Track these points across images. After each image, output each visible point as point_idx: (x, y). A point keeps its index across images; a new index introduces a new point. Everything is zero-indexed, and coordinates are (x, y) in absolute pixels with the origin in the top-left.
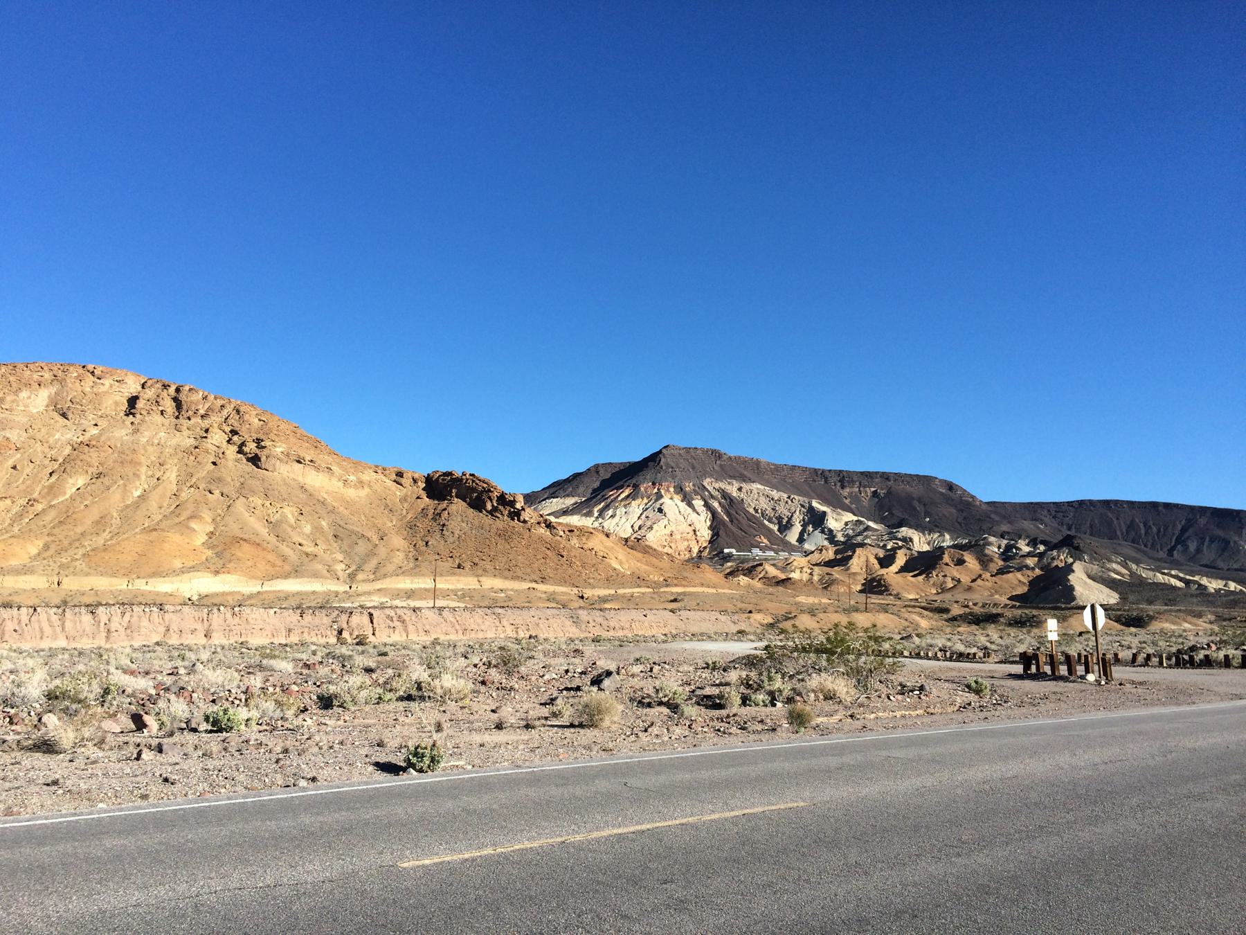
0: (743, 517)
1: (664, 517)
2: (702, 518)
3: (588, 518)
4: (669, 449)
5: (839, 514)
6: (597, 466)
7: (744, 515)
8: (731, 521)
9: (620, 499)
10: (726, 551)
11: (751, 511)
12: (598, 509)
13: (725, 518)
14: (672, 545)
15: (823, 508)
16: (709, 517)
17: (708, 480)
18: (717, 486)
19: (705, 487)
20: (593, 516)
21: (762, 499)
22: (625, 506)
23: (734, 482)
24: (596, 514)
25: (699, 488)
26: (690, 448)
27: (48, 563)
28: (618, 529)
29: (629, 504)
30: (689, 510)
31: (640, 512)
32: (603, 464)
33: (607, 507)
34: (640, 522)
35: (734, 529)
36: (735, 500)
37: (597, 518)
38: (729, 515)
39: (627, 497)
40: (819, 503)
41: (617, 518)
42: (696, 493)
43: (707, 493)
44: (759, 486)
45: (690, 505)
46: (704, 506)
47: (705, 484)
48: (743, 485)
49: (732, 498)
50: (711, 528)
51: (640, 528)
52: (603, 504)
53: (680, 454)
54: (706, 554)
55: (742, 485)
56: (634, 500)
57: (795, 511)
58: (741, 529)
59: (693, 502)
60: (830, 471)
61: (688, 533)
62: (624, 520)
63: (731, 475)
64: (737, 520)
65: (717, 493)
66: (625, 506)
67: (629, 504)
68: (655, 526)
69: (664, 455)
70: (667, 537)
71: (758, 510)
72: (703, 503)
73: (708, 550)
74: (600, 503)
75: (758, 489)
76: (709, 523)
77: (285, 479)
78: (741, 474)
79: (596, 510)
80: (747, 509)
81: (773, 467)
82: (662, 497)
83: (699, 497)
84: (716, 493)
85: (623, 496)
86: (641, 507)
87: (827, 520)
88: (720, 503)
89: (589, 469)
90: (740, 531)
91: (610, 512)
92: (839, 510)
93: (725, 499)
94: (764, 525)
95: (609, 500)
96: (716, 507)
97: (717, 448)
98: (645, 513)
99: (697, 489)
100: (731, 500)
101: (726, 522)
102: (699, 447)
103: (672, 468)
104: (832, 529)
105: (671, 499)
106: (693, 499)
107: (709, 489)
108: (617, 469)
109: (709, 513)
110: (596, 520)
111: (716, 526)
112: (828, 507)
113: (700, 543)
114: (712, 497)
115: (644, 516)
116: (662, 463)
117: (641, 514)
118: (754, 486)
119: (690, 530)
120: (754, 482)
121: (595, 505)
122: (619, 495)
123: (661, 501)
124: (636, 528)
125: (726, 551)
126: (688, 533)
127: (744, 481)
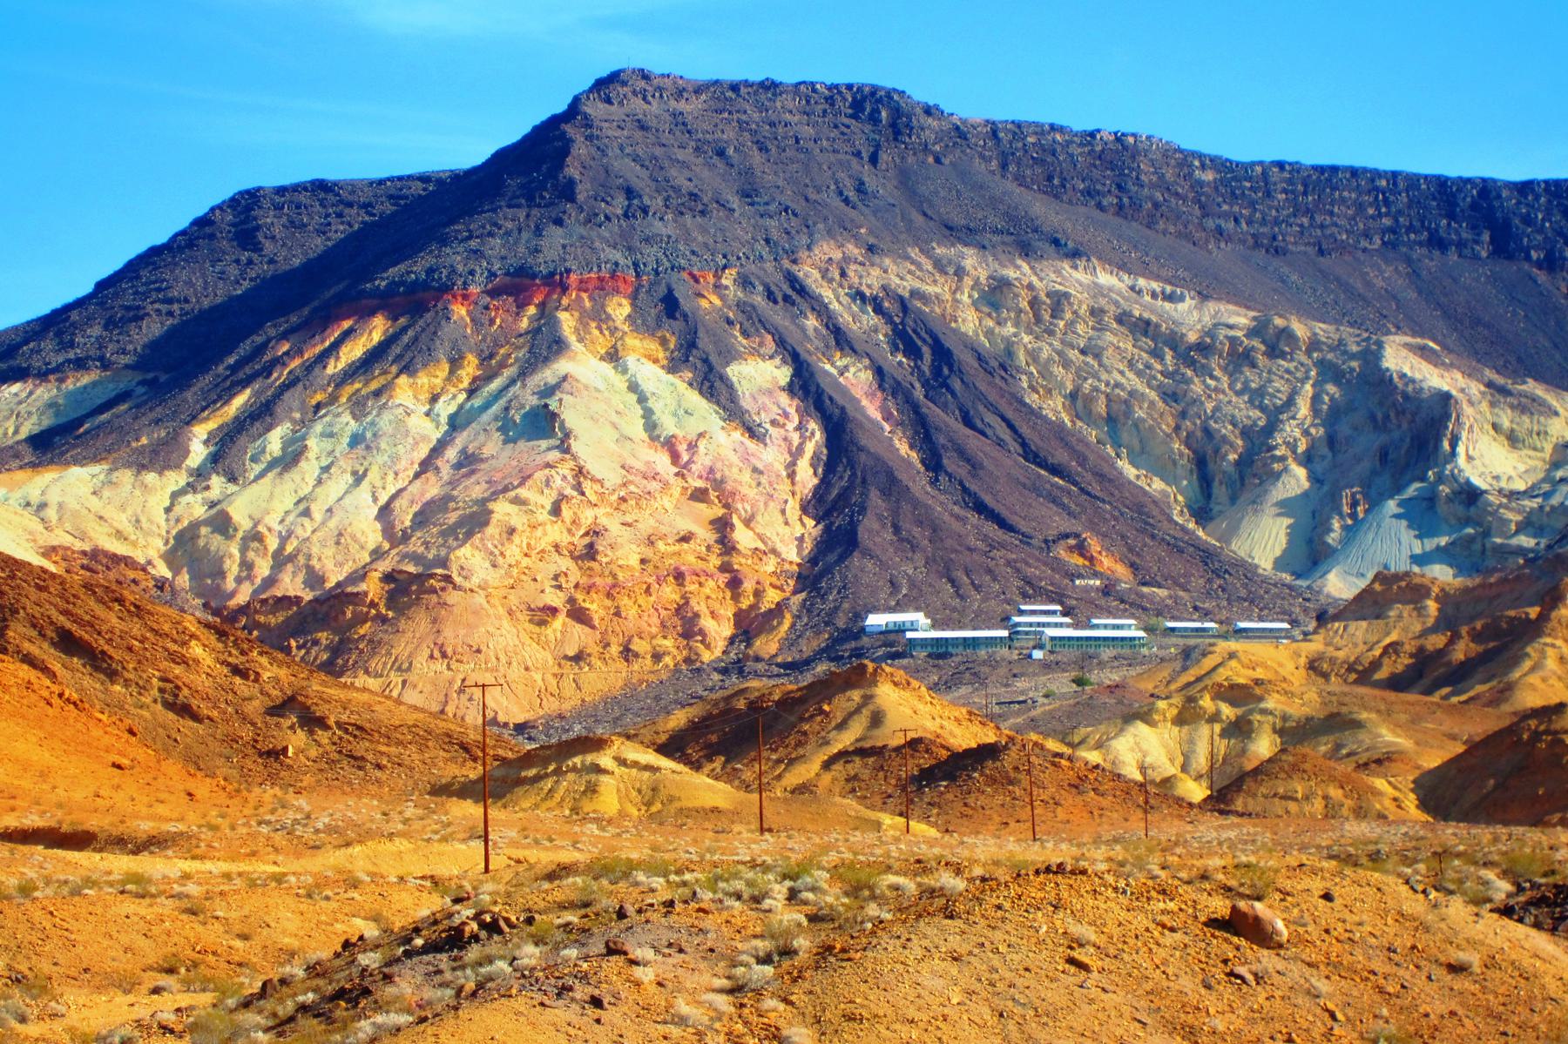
0: (1000, 443)
1: (554, 455)
2: (772, 456)
3: (150, 477)
4: (617, 91)
5: (1528, 406)
6: (246, 203)
7: (1005, 434)
8: (933, 463)
9: (334, 367)
10: (876, 620)
11: (1054, 408)
12: (212, 425)
13: (903, 448)
14: (595, 606)
15: (1435, 379)
16: (810, 448)
17: (827, 250)
18: (872, 280)
19: (802, 291)
20: (178, 466)
21: (1117, 341)
22: (358, 407)
23: (970, 259)
24: (198, 452)
25: (771, 296)
26: (735, 87)
27: (1336, 1026)
28: (305, 529)
29: (377, 394)
30: (704, 413)
31: (436, 435)
32: (281, 191)
33: (261, 415)
34: (432, 488)
35: (942, 504)
36: (966, 358)
37: (200, 474)
38: (923, 433)
39: (374, 357)
40: (1423, 352)
41: (309, 468)
42: (752, 321)
43: (812, 322)
44: (1105, 278)
45: (713, 384)
46: (790, 389)
47: (809, 273)
48: (1020, 271)
49: (948, 343)
50: (820, 505)
51: (423, 518)
52: (240, 401)
53: (677, 118)
54: (773, 647)
55: (1011, 273)
56: (408, 369)
57: (1290, 402)
58: (980, 508)
59: (734, 371)
60: (1525, 188)
61: (685, 539)
62: (339, 483)
63: (959, 220)
64: (962, 453)
65: (870, 319)
66: (358, 407)
67: (377, 394)
68: (502, 509)
69: (588, 123)
70: (565, 563)
71: (1089, 400)
72: (784, 374)
73: (787, 621)
74: (226, 395)
75: (1098, 291)
76: (807, 478)
77: (732, 598)
78: (1010, 217)
79: (201, 431)
80: (1032, 399)
81: (1209, 176)
82: (558, 346)
83: (770, 345)
84: (862, 323)
85: (353, 351)
86: (446, 408)
87: (1454, 443)
88: (879, 372)
89: (201, 222)
90: (973, 518)
91: (274, 442)
92: (1532, 387)
93: (912, 351)
94: (1111, 480)
95: (280, 376)
96: (858, 393)
97: (886, 81)
98: (461, 440)
99: (759, 300)
100: (942, 354)
101: (902, 476)
102: (787, 76)
103: (630, 193)
104: (1477, 481)
105: (613, 356)
106: (731, 355)
107: (827, 294)
108: (357, 218)
109: (813, 425)
110: (191, 488)
111: (844, 495)
112: (1469, 375)
113: (748, 586)
114: (840, 338)
115: (451, 454)
116: (572, 170)
117: (438, 450)
118: (1079, 275)
119: (697, 520)
120: (1075, 255)
121: (193, 418)
122: (336, 345)
123: (548, 375)
124: (404, 516)
125: (876, 620)
126: (685, 539)
127: (1026, 251)
